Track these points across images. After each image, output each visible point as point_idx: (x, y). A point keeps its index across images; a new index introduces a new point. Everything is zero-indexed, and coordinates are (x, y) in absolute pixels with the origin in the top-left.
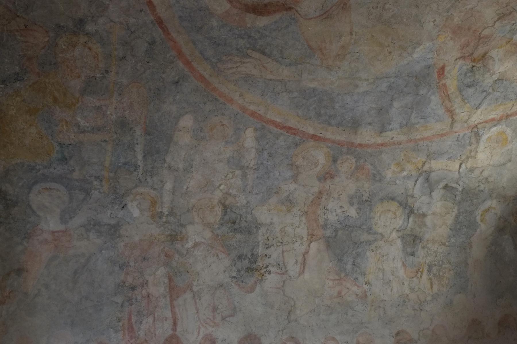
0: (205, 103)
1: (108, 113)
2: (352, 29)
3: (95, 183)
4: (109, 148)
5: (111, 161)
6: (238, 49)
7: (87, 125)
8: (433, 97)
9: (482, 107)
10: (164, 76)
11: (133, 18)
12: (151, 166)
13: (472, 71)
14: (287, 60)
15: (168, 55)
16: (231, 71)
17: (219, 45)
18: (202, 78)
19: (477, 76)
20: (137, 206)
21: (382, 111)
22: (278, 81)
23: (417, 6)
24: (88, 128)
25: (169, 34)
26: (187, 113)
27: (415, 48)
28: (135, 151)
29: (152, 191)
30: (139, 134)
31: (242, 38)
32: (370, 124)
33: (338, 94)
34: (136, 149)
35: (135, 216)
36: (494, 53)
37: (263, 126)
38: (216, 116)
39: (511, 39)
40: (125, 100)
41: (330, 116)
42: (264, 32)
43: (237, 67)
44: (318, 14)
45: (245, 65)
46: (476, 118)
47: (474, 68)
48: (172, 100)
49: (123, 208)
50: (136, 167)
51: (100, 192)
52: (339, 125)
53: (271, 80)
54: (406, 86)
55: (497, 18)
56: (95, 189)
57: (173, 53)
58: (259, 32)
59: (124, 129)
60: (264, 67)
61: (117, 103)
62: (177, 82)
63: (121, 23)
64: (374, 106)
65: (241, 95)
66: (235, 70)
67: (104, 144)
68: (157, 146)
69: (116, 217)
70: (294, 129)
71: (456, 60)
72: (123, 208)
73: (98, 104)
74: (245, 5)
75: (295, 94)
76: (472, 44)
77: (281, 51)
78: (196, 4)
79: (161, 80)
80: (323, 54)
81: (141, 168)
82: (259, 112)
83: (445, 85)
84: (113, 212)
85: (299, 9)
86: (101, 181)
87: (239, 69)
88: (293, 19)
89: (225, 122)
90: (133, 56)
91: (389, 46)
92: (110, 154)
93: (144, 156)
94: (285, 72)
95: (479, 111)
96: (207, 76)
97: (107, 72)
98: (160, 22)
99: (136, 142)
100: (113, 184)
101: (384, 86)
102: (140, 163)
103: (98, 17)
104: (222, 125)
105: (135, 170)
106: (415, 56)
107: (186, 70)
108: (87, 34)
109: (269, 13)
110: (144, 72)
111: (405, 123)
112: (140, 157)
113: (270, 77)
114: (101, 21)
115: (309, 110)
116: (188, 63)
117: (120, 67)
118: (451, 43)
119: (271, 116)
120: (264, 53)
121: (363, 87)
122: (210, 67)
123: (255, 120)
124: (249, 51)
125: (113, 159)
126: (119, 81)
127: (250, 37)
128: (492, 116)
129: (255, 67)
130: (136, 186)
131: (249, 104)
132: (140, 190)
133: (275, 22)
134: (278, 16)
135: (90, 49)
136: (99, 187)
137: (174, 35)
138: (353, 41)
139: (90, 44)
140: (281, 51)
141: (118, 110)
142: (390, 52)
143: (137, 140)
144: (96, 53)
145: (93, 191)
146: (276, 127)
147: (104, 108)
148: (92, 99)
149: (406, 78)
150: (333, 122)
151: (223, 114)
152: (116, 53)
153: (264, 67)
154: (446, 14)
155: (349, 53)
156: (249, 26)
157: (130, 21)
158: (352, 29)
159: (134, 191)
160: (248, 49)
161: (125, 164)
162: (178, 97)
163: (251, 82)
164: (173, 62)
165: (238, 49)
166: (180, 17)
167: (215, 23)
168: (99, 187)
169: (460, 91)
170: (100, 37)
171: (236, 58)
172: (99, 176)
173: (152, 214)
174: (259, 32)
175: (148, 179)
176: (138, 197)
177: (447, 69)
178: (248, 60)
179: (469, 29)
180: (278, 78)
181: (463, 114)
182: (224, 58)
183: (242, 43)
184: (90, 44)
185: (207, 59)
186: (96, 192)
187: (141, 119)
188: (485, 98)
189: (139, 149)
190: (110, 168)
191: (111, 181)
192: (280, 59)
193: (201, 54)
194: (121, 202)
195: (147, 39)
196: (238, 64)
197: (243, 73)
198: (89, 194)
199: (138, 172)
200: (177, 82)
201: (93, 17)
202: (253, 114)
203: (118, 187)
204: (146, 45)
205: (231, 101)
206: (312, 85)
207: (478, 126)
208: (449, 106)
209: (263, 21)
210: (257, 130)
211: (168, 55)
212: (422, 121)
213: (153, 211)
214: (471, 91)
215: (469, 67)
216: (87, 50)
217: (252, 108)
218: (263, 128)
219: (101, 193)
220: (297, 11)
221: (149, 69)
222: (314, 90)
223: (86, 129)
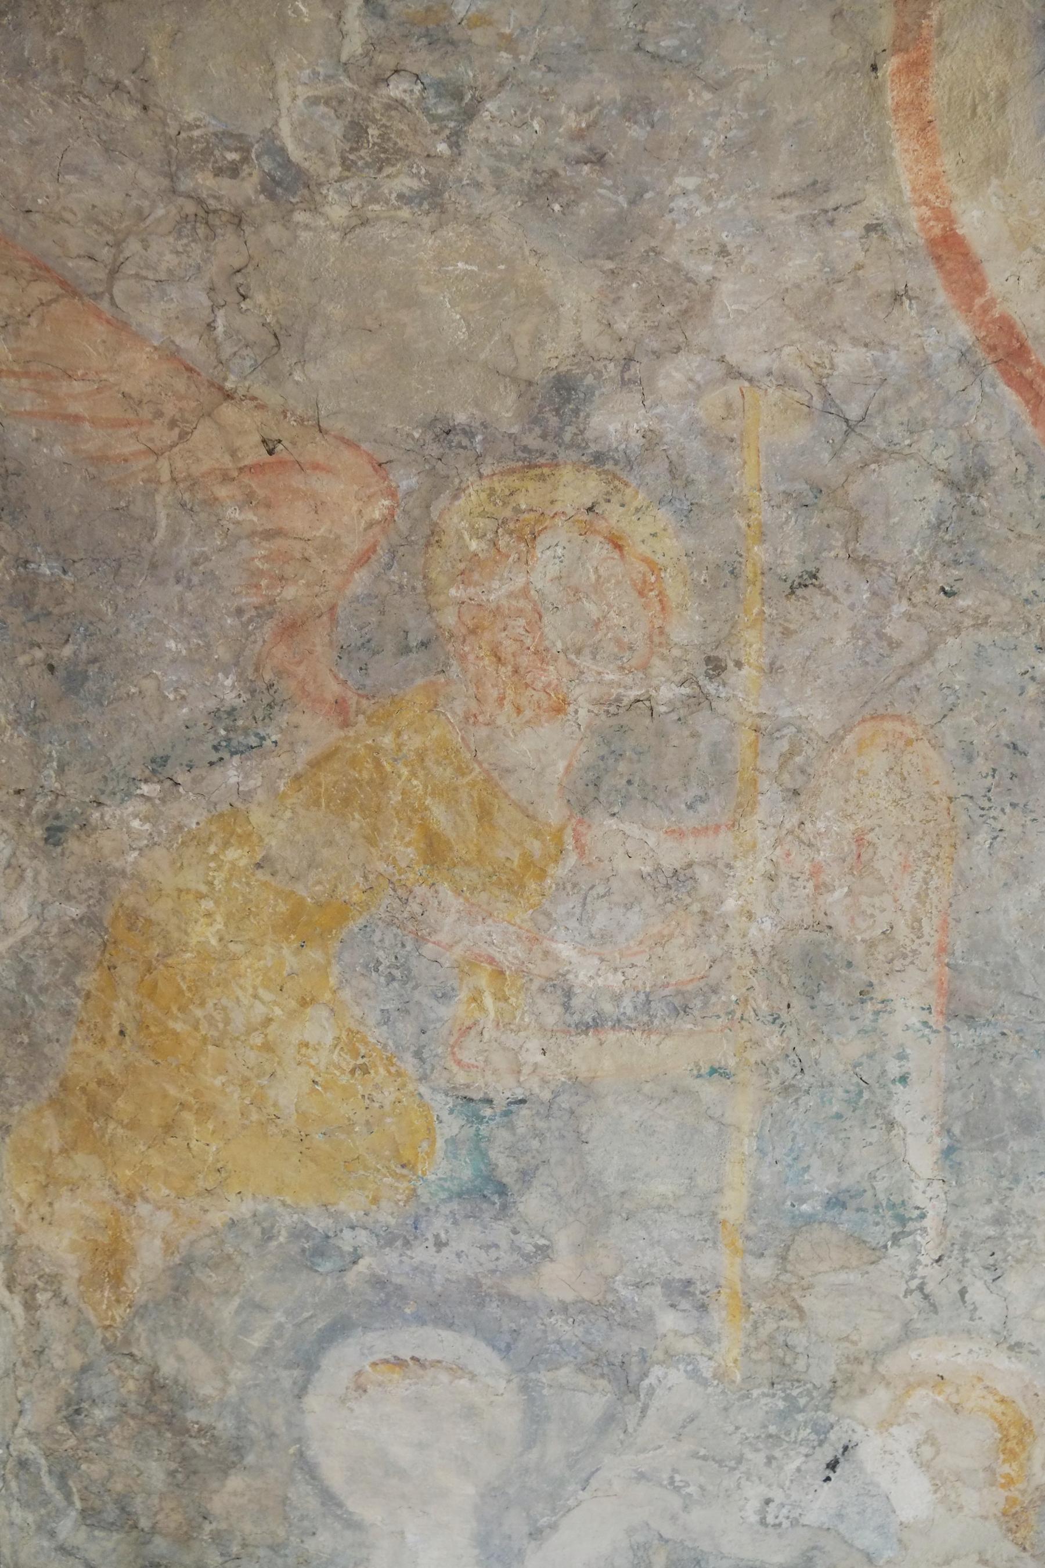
1: (731, 904)
3: (668, 1321)
4: (742, 1108)
5: (758, 1188)
7: (615, 981)
11: (855, 341)
12: (988, 1211)
20: (915, 1452)
24: (617, 998)
28: (891, 1124)
29: (1002, 1361)
30: (914, 1020)
34: (896, 1112)
35: (906, 1514)
40: (821, 825)
49: (833, 1465)
50: (902, 1220)
51: (694, 1374)
56: (670, 1357)
59: (824, 996)
61: (778, 842)
63: (786, 380)
67: (709, 1091)
68: (1020, 1088)
69: (795, 1523)
72: (833, 1465)
73: (671, 857)
81: (927, 1222)
84: (778, 1495)
86: (703, 1307)
90: (861, 562)
92: (749, 1145)
93: (948, 1152)
97: (715, 667)
99: (894, 1069)
100: (770, 1325)
102: (927, 1195)
103: (657, 355)
105: (895, 1239)
108: (598, 458)
110: (929, 653)
112: (921, 1155)
114: (674, 376)
117: (787, 633)
125: (766, 1178)
126: (786, 714)
130: (908, 1334)
132: (931, 1354)
135: (616, 543)
136: (691, 1345)
139: (614, 516)
141: (784, 882)
143: (902, 1057)
144: (654, 567)
145: (657, 1371)
147: (704, 876)
148: (634, 830)
152: (760, 553)
157: (839, 359)
159: (894, 1364)
161: (837, 1202)
168: (691, 1345)
170: (673, 471)
172: (689, 1282)
173: (1011, 1501)
175: (977, 1292)
176: (921, 1400)
184: (614, 516)
186: (676, 1376)
187: (916, 928)
189: (916, 1108)
190: (751, 1230)
191: (758, 1306)
194: (822, 1432)
195: (939, 457)
198: (635, 1391)
199: (915, 1247)
201: (629, 359)
203: (800, 1340)
204: (934, 491)
213: (1010, 1482)
216: (599, 550)
219: (705, 1383)
221: (958, 629)
223: (608, 1007)
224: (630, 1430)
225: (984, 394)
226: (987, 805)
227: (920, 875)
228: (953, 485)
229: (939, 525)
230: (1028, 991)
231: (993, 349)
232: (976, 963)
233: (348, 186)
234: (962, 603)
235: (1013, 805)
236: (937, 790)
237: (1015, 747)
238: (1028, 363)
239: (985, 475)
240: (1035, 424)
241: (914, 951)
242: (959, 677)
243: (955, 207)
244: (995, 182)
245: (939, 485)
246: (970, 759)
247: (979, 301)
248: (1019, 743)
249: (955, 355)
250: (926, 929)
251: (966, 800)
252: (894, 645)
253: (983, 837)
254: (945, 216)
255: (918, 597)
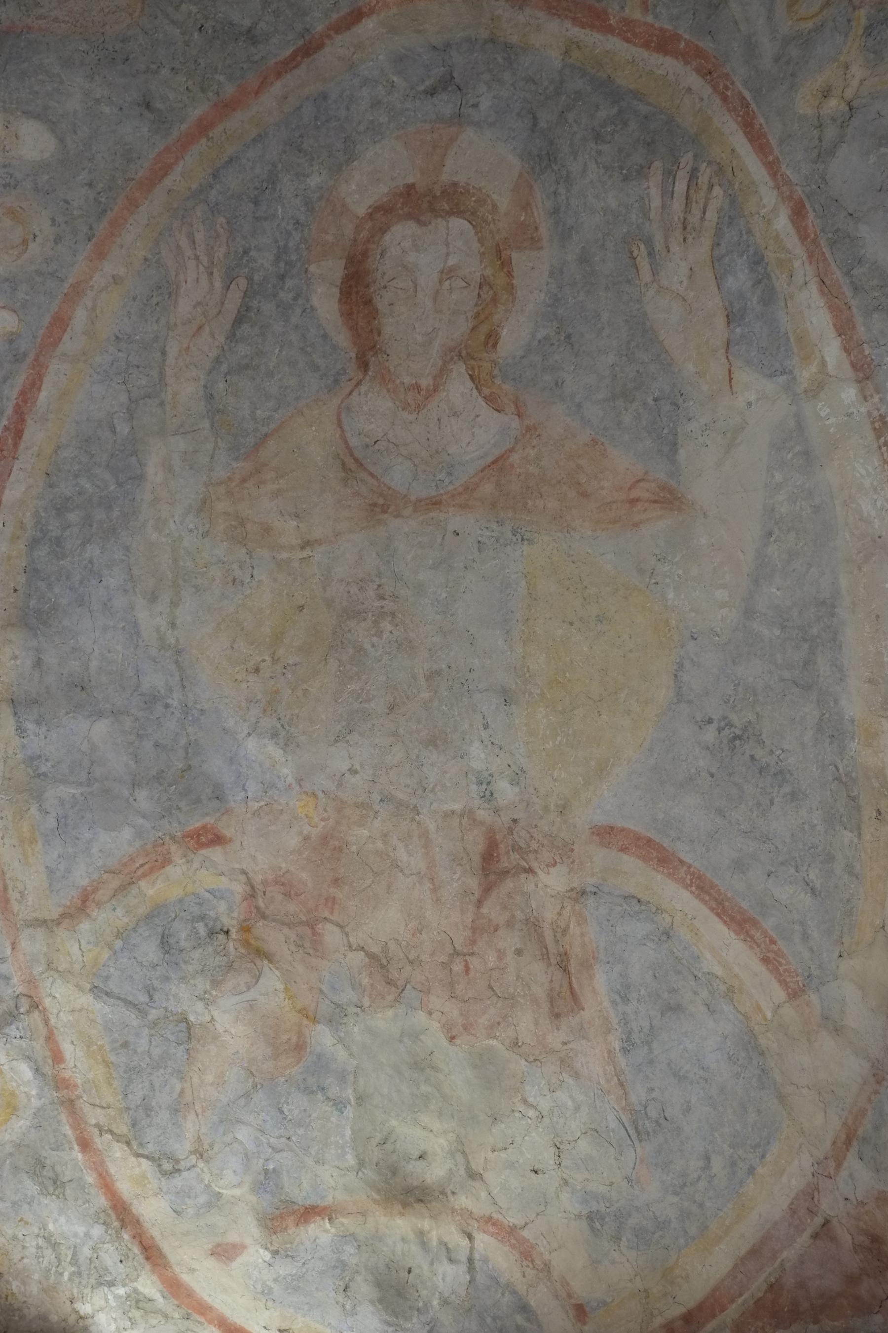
0: (90, 185)
2: (319, 542)
6: (246, 252)
8: (127, 833)
9: (99, 1005)
10: (165, 72)
13: (212, 933)
14: (222, 385)
15: (222, 78)
16: (184, 242)
17: (256, 202)
18: (162, 170)
19: (196, 954)
21: (79, 692)
22: (162, 375)
23: (392, 708)
25: (279, 75)
26: (61, 140)
27: (275, 735)
31: (278, 258)
32: (38, 663)
33: (127, 549)
36: (271, 980)
37: (25, 355)
38: (53, 220)
39: (315, 1020)
41: (58, 541)
42: (298, 311)
43: (197, 258)
44: (354, 442)
45: (204, 278)
46: (64, 1000)
47: (222, 937)
48: (98, 96)
52: (32, 572)
53: (164, 353)
54: (157, 745)
55: (375, 949)
57: (229, 90)
58: (295, 299)
60: (200, 328)
62: (148, 106)
64: (94, 664)
65: (116, 280)
66: (188, 253)
70: (16, 445)
71: (244, 872)
74: (365, 254)
75: (123, 429)
76: (292, 907)
77: (247, 367)
78: (362, 128)
79: (154, 67)
80: (244, 480)
82: (66, 337)
83: (167, 861)
85: (363, 388)
87: (191, 264)
88: (336, 381)
89: (34, 248)
91: (275, 661)
94: (186, 390)
95: (87, 1000)
96: (168, 182)
98: (309, 49)
101: (154, 680)
104: (25, 242)
106: (251, 744)
107: (184, 127)
109: (348, 315)
110: (173, 22)
111: (43, 769)
113: (173, 350)
115: (76, 476)
116: (204, 127)
118: (293, 841)
119: (57, 373)
120: (239, 320)
121: (150, 620)
122: (194, 186)
123: (41, 332)
124: (243, 283)
127: (282, 277)
128: (67, 1049)
129: (199, 303)
131: (90, 304)
133: (325, 336)
134: (342, 338)
137: (277, 88)
138: (285, 555)
140: (247, 367)
142: (257, 670)
146: (23, 393)
149: (183, 741)
150: (42, 552)
151: (58, 239)
153: (200, 328)
154: (376, 797)
155: (250, 553)
156: (312, 268)
158: (319, 542)
160: (250, 279)
162: (107, 110)
163: (155, 300)
164: (203, 90)
165: (246, 252)
166: (325, 96)
167: (314, 181)
169: (149, 918)
171: (223, 249)
174: (295, 299)
177: (216, 854)
178: (218, 284)
179: (336, 881)
180: (169, 372)
181: (75, 950)
182: (222, 220)
183: (265, 260)
185: (215, 176)
187: (40, 17)
188: (129, 1003)
192: (224, 367)
193: (231, 161)
195: (262, 25)
196: (204, 259)
197: (182, 277)
200: (148, 106)
202: (60, 323)
204: (247, 23)
205: (100, 254)
206: (153, 471)
207: (36, 1014)
208: (100, 895)
209: (325, 303)
210: (11, 342)
211: (222, 78)
212: (51, 822)
214: (150, 950)
215: (226, 922)
217: (80, 317)
218: (18, 358)
220: (359, 384)
221: (183, 34)
222: (140, 478)
224: (86, 741)
225: (289, 41)
226: (100, 48)
227: (67, 19)
228: (249, 31)
229: (231, 24)
230: (8, 67)
231: (310, 43)
232: (22, 44)
233: (57, 1193)
234: (196, 35)
235: (99, 60)
236: (108, 27)
237: (127, 60)
238: (303, 58)
239: (253, 44)
240: (276, 63)
241: (29, 15)
242: (161, 35)
243: (374, 17)
244: (385, 31)
245: (249, 25)
246: (123, 41)
247: (332, 33)
248: (129, 62)
249: (308, 26)
250: (40, 22)
251: (102, 40)
252: (177, 8)
253: (84, 47)
254: (372, 11)
255: (199, 16)
